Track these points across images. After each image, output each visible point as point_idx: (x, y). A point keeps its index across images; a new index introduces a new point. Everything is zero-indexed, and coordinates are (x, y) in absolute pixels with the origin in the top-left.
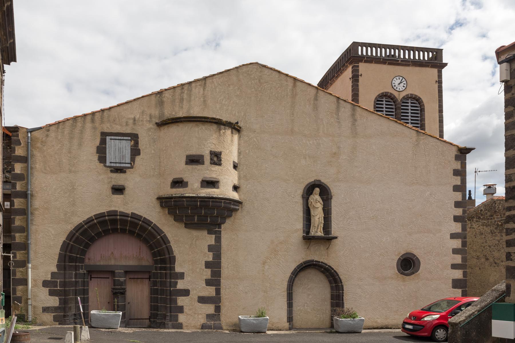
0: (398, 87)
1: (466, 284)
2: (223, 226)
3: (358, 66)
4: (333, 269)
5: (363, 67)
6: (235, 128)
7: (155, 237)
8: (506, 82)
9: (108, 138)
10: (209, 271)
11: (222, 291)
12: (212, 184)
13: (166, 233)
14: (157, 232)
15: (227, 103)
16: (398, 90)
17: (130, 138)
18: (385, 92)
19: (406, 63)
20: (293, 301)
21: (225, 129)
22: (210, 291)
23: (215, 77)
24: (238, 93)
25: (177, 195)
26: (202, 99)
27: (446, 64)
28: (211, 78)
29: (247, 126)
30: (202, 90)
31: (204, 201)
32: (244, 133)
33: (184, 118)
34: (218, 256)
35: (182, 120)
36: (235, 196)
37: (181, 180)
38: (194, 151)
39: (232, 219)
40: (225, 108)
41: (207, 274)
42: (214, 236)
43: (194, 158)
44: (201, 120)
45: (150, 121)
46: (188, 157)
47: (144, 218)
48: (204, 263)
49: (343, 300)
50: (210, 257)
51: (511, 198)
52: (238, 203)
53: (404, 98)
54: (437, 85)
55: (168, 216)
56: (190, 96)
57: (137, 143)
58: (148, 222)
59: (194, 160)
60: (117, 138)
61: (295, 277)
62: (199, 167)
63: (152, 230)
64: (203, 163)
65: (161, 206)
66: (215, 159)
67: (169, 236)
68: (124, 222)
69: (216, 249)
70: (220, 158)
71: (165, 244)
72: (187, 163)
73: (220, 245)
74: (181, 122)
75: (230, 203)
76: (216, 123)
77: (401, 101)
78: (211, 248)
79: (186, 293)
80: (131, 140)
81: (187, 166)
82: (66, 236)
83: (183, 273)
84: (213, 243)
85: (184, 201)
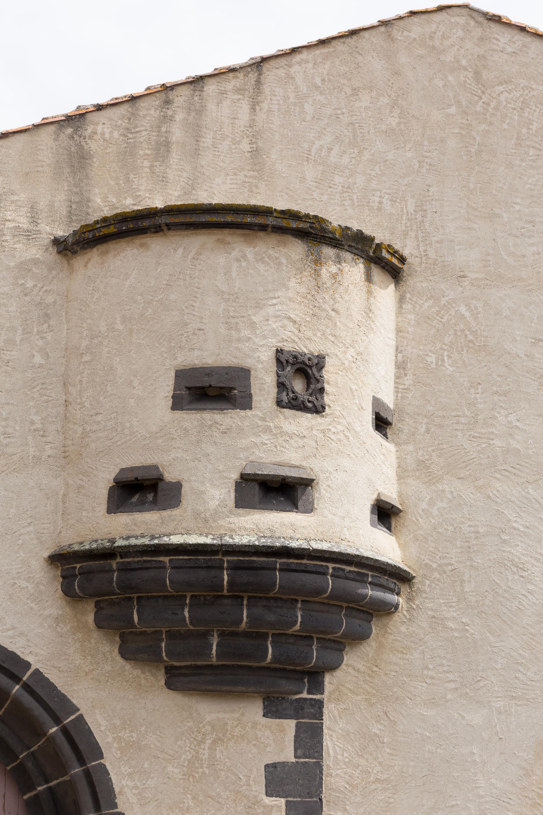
1: (271, 731)
6: (386, 263)
7: (38, 732)
12: (283, 491)
13: (83, 711)
15: (345, 160)
21: (339, 261)
23: (297, 58)
24: (393, 122)
25: (133, 541)
26: (245, 146)
28: (283, 61)
29: (432, 254)
30: (245, 106)
31: (251, 568)
32: (416, 281)
33: (170, 211)
37: (153, 475)
38: (209, 353)
39: (369, 648)
40: (338, 179)
43: (206, 382)
44: (239, 219)
45: (29, 235)
46: (181, 375)
52: (398, 577)
55: (96, 634)
56: (196, 131)
59: (209, 390)
62: (230, 418)
63: (28, 700)
64: (245, 402)
65: (68, 591)
66: (298, 385)
67: (101, 726)
72: (177, 404)
73: (319, 766)
74: (157, 230)
75: (361, 579)
76: (302, 234)
81: (179, 414)
84: (287, 754)
85: (162, 567)
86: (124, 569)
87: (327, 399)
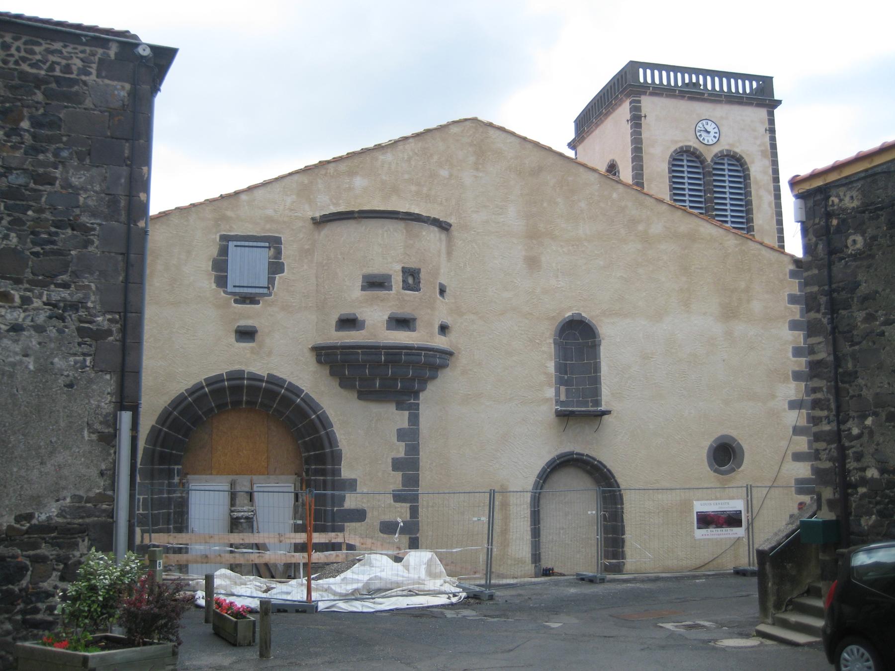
0: (706, 139)
2: (422, 395)
3: (639, 102)
4: (605, 467)
5: (648, 104)
8: (803, 223)
9: (231, 244)
10: (399, 475)
11: (422, 512)
14: (311, 408)
16: (706, 142)
17: (267, 244)
18: (686, 146)
19: (716, 98)
20: (542, 526)
22: (400, 514)
27: (779, 102)
34: (413, 449)
35: (356, 215)
36: (440, 342)
37: (352, 317)
38: (377, 268)
39: (438, 382)
41: (396, 480)
42: (406, 413)
43: (375, 280)
47: (290, 383)
48: (390, 461)
49: (622, 521)
50: (400, 450)
51: (815, 376)
53: (716, 156)
54: (768, 135)
57: (278, 253)
58: (294, 390)
59: (375, 283)
60: (247, 244)
61: (544, 482)
63: (303, 405)
65: (319, 361)
68: (254, 390)
69: (410, 436)
70: (419, 278)
71: (325, 429)
73: (418, 429)
74: (355, 218)
77: (712, 160)
78: (402, 435)
79: (359, 515)
80: (269, 247)
82: (155, 417)
83: (355, 480)
84: (405, 424)
85: (358, 353)
86: (342, 354)
87: (421, 285)
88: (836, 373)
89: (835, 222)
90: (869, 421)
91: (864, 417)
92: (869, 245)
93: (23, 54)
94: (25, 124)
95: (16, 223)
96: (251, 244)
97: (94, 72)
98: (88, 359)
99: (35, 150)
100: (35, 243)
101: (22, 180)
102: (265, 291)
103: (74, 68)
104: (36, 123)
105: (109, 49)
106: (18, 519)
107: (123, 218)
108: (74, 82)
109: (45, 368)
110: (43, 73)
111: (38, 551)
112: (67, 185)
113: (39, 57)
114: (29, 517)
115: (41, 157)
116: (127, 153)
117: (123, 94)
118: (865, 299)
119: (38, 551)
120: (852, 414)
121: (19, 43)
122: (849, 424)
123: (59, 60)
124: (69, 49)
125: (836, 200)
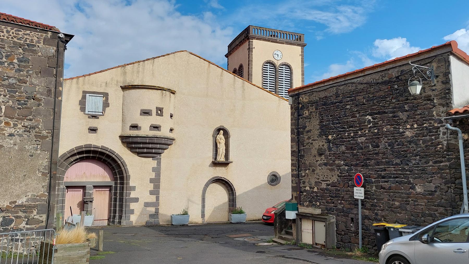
26: (151, 72)
30: (152, 66)
38: (146, 107)
50: (153, 175)
56: (144, 69)
57: (107, 99)
59: (146, 113)
62: (149, 117)
69: (157, 171)
78: (154, 169)
88: (298, 155)
89: (301, 106)
90: (307, 172)
91: (306, 170)
92: (310, 115)
93: (15, 35)
94: (16, 61)
95: (12, 97)
96: (96, 95)
97: (42, 42)
98: (39, 146)
99: (20, 71)
100: (19, 104)
101: (14, 81)
102: (101, 114)
103: (34, 41)
104: (20, 60)
105: (48, 34)
106: (10, 203)
107: (53, 96)
108: (34, 46)
109: (22, 149)
110: (22, 42)
111: (18, 215)
112: (32, 84)
113: (21, 36)
114: (16, 202)
115: (22, 73)
116: (55, 73)
117: (53, 51)
118: (308, 132)
119: (18, 215)
120: (303, 169)
121: (13, 31)
122: (301, 172)
123: (28, 37)
124: (32, 33)
125: (301, 99)
